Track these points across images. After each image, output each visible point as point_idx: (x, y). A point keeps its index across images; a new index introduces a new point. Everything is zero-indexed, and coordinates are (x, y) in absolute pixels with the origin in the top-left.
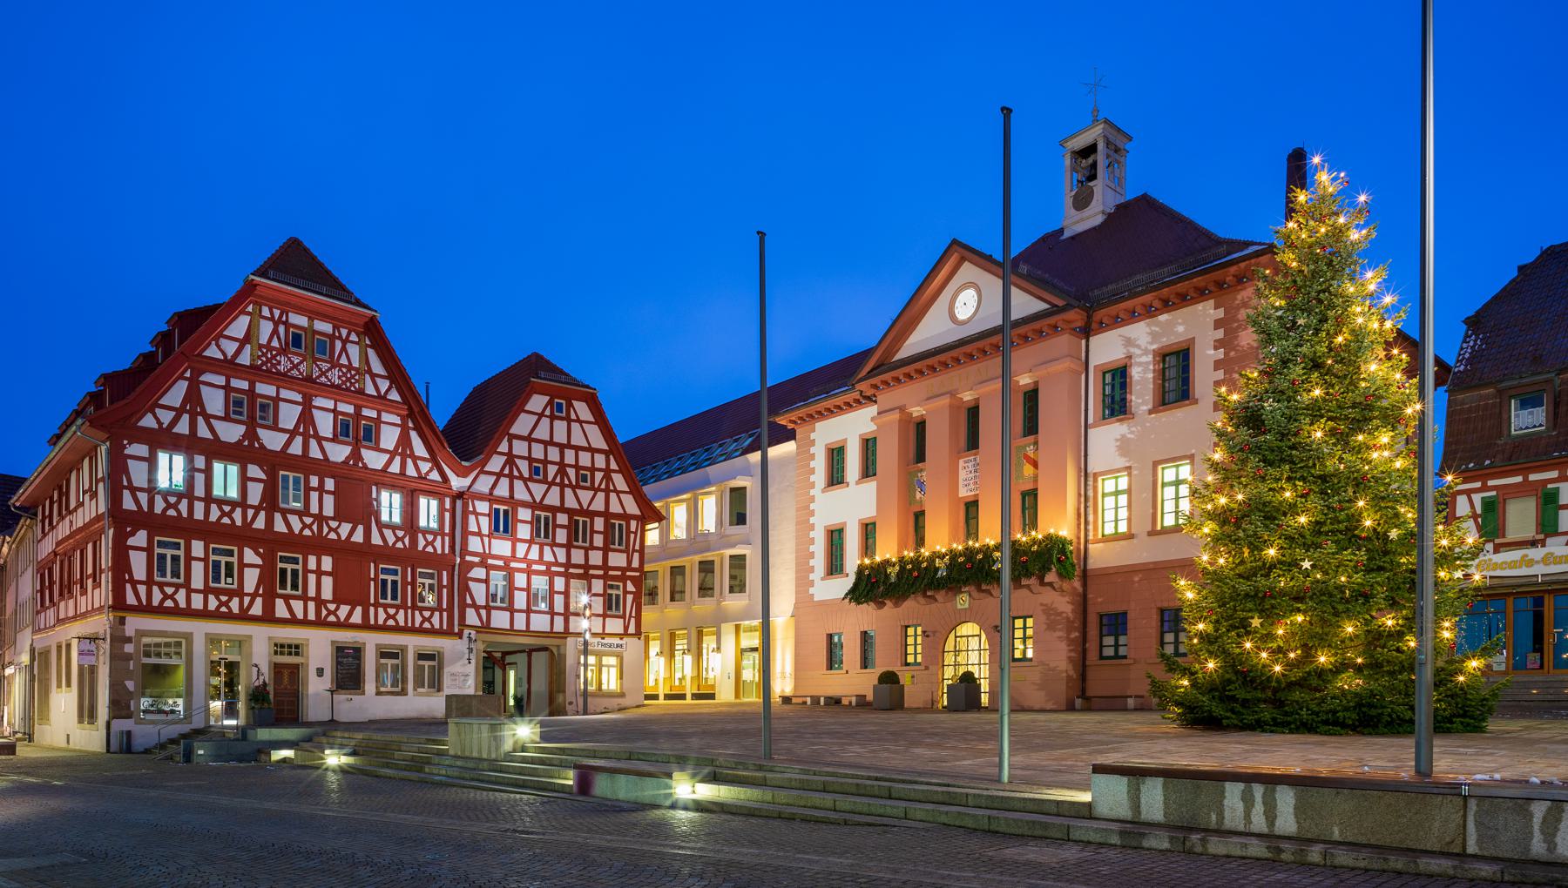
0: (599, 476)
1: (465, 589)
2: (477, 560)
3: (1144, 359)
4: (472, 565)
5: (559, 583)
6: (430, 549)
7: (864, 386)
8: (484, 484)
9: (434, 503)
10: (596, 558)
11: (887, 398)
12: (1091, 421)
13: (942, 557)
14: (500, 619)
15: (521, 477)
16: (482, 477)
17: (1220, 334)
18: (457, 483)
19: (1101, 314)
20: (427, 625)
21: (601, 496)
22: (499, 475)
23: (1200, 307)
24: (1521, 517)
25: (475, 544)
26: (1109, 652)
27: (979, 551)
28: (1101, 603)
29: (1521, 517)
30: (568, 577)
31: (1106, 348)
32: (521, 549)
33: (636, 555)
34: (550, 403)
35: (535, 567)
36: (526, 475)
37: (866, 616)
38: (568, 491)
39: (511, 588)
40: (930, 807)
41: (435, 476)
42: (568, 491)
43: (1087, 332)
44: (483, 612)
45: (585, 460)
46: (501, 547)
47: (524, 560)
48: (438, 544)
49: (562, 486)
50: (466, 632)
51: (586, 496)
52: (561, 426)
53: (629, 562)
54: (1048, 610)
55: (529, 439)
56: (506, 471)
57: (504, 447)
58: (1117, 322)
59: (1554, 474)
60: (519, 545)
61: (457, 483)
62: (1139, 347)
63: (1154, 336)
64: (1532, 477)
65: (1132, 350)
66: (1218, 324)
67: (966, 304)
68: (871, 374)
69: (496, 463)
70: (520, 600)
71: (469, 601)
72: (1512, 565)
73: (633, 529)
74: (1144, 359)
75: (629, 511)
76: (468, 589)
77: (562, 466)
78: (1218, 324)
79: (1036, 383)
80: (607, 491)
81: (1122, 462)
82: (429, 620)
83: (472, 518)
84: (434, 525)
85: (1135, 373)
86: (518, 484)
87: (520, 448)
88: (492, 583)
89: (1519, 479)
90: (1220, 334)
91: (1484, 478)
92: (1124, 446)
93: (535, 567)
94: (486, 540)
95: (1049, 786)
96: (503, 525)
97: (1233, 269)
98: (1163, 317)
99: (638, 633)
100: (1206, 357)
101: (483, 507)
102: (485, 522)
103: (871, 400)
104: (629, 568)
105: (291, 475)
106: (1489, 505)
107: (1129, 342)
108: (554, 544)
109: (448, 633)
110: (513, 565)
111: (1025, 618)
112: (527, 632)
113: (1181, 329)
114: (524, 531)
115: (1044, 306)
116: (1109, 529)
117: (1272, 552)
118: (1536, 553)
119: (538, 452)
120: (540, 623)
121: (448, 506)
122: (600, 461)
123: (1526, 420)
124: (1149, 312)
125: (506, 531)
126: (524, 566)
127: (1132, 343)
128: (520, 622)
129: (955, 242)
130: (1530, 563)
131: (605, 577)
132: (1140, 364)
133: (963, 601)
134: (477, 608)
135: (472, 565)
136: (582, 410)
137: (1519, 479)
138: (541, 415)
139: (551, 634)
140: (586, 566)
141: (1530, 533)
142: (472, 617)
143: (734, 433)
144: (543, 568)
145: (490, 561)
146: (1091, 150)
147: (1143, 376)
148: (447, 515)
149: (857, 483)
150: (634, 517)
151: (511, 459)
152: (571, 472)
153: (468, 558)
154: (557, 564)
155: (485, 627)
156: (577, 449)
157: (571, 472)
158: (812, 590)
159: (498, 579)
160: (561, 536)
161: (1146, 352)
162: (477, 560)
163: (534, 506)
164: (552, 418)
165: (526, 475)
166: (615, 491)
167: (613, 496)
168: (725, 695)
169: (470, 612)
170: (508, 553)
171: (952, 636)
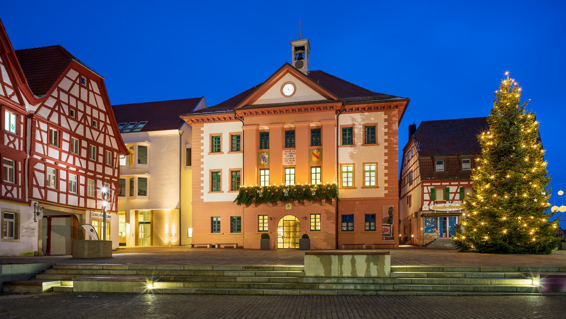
0: (102, 124)
1: (32, 175)
2: (39, 158)
3: (359, 126)
4: (37, 161)
5: (82, 180)
6: (11, 146)
7: (240, 113)
8: (44, 113)
9: (13, 117)
10: (99, 169)
11: (247, 120)
12: (339, 145)
13: (286, 188)
14: (52, 196)
15: (64, 114)
16: (43, 108)
17: (386, 124)
18: (29, 108)
19: (348, 107)
20: (9, 195)
22: (53, 110)
23: (379, 113)
24: (440, 195)
25: (39, 148)
26: (367, 228)
27: (304, 187)
28: (344, 211)
29: (440, 195)
30: (86, 177)
31: (345, 120)
32: (64, 156)
33: (116, 170)
35: (71, 168)
36: (67, 114)
37: (245, 212)
39: (57, 179)
41: (15, 99)
42: (87, 129)
43: (339, 112)
44: (43, 191)
45: (95, 114)
46: (54, 153)
47: (66, 163)
48: (17, 143)
49: (85, 126)
50: (33, 202)
51: (95, 134)
52: (84, 91)
54: (327, 212)
55: (68, 93)
56: (57, 109)
57: (55, 94)
58: (351, 111)
59: (448, 184)
60: (63, 154)
61: (29, 108)
62: (357, 122)
63: (363, 120)
64: (443, 184)
65: (355, 123)
66: (386, 120)
67: (289, 90)
68: (243, 108)
69: (51, 102)
70: (63, 186)
71: (35, 183)
72: (442, 208)
74: (359, 126)
76: (34, 175)
77: (85, 115)
78: (386, 120)
79: (295, 128)
81: (352, 162)
82: (10, 192)
83: (38, 132)
84: (13, 131)
85: (356, 131)
86: (63, 118)
87: (64, 97)
88: (48, 174)
89: (440, 184)
90: (386, 124)
91: (431, 182)
92: (352, 156)
94: (45, 147)
95: (505, 277)
96: (55, 140)
97: (394, 103)
98: (366, 114)
99: (116, 211)
100: (381, 132)
102: (45, 136)
103: (241, 119)
104: (113, 176)
106: (432, 190)
107: (353, 119)
108: (80, 157)
109: (22, 201)
110: (60, 165)
111: (315, 215)
112: (66, 205)
113: (373, 119)
114: (65, 146)
115: (323, 98)
116: (345, 185)
117: (525, 195)
118: (442, 205)
119: (73, 102)
120: (73, 200)
121: (22, 121)
122: (102, 117)
123: (440, 168)
124: (364, 110)
125: (55, 144)
126: (65, 167)
127: (356, 120)
128: (63, 197)
130: (446, 208)
132: (358, 128)
133: (289, 206)
134: (39, 188)
135: (37, 161)
136: (94, 86)
137: (440, 184)
138: (75, 82)
139: (77, 208)
140: (95, 172)
141: (442, 200)
142: (36, 193)
143: (139, 120)
144: (75, 169)
145: (48, 161)
146: (302, 48)
147: (359, 133)
148: (22, 126)
149: (229, 153)
151: (59, 102)
152: (89, 119)
153: (35, 156)
155: (44, 200)
156: (92, 107)
158: (202, 197)
159: (50, 171)
160: (84, 153)
161: (360, 124)
162: (39, 158)
163: (72, 133)
165: (67, 114)
166: (108, 134)
168: (131, 244)
169: (35, 190)
171: (282, 220)
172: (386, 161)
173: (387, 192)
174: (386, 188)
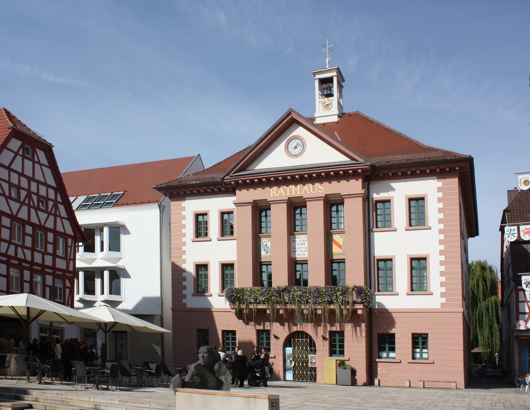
0: (51, 204)
34: (22, 146)
38: (33, 211)
40: (84, 399)
42: (33, 211)
45: (43, 190)
49: (29, 207)
52: (28, 164)
53: (68, 266)
73: (70, 244)
75: (67, 232)
77: (29, 193)
80: (55, 216)
93: (12, 261)
105: (40, 232)
108: (23, 247)
129: (410, 200)
131: (54, 275)
136: (41, 155)
138: (16, 154)
150: (70, 236)
152: (35, 197)
154: (25, 261)
156: (39, 182)
157: (35, 197)
158: (184, 301)
164: (24, 157)
166: (60, 216)
170: (64, 268)
172: (441, 253)
173: (444, 300)
174: (442, 295)
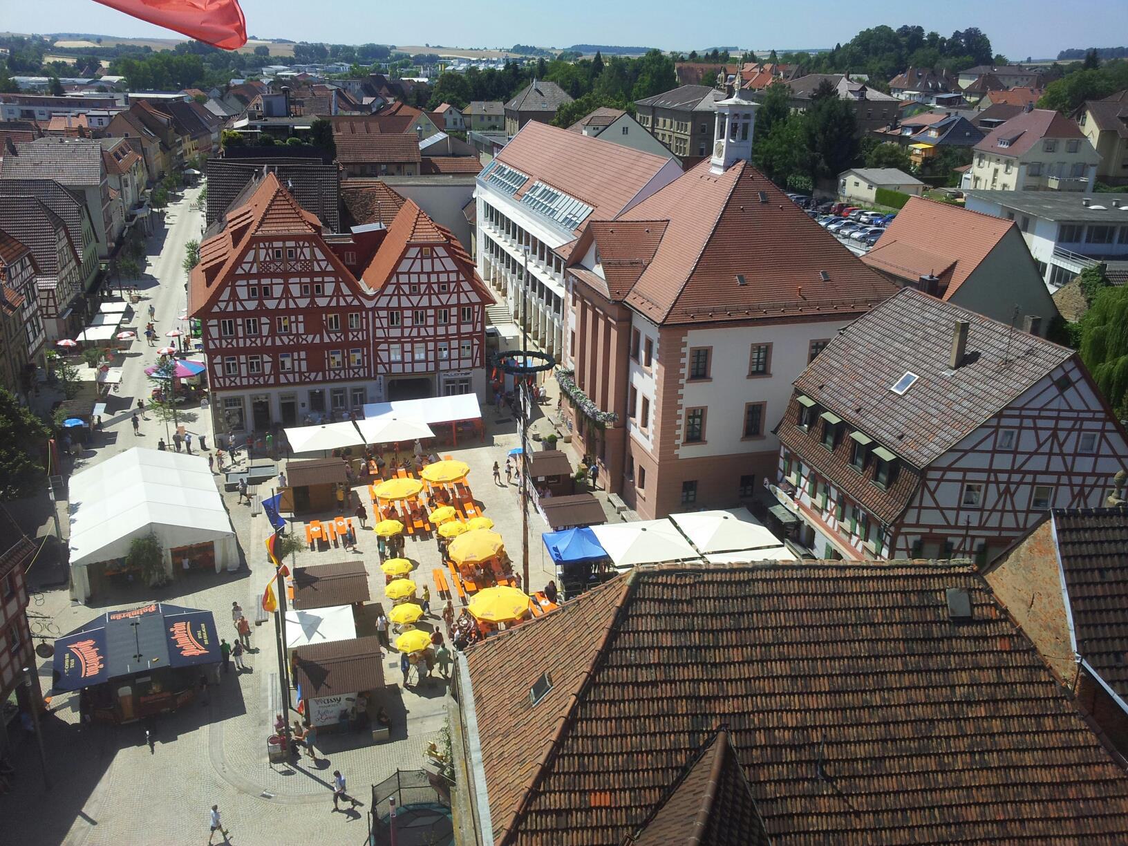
21: (455, 296)
51: (444, 298)
77: (429, 284)
101: (431, 312)
152: (435, 287)
156: (438, 273)
167: (462, 295)
